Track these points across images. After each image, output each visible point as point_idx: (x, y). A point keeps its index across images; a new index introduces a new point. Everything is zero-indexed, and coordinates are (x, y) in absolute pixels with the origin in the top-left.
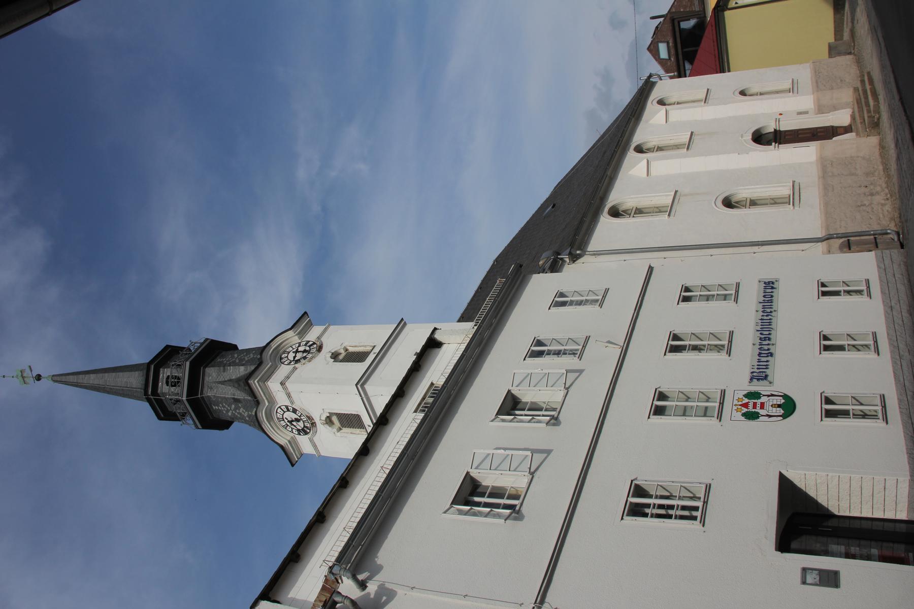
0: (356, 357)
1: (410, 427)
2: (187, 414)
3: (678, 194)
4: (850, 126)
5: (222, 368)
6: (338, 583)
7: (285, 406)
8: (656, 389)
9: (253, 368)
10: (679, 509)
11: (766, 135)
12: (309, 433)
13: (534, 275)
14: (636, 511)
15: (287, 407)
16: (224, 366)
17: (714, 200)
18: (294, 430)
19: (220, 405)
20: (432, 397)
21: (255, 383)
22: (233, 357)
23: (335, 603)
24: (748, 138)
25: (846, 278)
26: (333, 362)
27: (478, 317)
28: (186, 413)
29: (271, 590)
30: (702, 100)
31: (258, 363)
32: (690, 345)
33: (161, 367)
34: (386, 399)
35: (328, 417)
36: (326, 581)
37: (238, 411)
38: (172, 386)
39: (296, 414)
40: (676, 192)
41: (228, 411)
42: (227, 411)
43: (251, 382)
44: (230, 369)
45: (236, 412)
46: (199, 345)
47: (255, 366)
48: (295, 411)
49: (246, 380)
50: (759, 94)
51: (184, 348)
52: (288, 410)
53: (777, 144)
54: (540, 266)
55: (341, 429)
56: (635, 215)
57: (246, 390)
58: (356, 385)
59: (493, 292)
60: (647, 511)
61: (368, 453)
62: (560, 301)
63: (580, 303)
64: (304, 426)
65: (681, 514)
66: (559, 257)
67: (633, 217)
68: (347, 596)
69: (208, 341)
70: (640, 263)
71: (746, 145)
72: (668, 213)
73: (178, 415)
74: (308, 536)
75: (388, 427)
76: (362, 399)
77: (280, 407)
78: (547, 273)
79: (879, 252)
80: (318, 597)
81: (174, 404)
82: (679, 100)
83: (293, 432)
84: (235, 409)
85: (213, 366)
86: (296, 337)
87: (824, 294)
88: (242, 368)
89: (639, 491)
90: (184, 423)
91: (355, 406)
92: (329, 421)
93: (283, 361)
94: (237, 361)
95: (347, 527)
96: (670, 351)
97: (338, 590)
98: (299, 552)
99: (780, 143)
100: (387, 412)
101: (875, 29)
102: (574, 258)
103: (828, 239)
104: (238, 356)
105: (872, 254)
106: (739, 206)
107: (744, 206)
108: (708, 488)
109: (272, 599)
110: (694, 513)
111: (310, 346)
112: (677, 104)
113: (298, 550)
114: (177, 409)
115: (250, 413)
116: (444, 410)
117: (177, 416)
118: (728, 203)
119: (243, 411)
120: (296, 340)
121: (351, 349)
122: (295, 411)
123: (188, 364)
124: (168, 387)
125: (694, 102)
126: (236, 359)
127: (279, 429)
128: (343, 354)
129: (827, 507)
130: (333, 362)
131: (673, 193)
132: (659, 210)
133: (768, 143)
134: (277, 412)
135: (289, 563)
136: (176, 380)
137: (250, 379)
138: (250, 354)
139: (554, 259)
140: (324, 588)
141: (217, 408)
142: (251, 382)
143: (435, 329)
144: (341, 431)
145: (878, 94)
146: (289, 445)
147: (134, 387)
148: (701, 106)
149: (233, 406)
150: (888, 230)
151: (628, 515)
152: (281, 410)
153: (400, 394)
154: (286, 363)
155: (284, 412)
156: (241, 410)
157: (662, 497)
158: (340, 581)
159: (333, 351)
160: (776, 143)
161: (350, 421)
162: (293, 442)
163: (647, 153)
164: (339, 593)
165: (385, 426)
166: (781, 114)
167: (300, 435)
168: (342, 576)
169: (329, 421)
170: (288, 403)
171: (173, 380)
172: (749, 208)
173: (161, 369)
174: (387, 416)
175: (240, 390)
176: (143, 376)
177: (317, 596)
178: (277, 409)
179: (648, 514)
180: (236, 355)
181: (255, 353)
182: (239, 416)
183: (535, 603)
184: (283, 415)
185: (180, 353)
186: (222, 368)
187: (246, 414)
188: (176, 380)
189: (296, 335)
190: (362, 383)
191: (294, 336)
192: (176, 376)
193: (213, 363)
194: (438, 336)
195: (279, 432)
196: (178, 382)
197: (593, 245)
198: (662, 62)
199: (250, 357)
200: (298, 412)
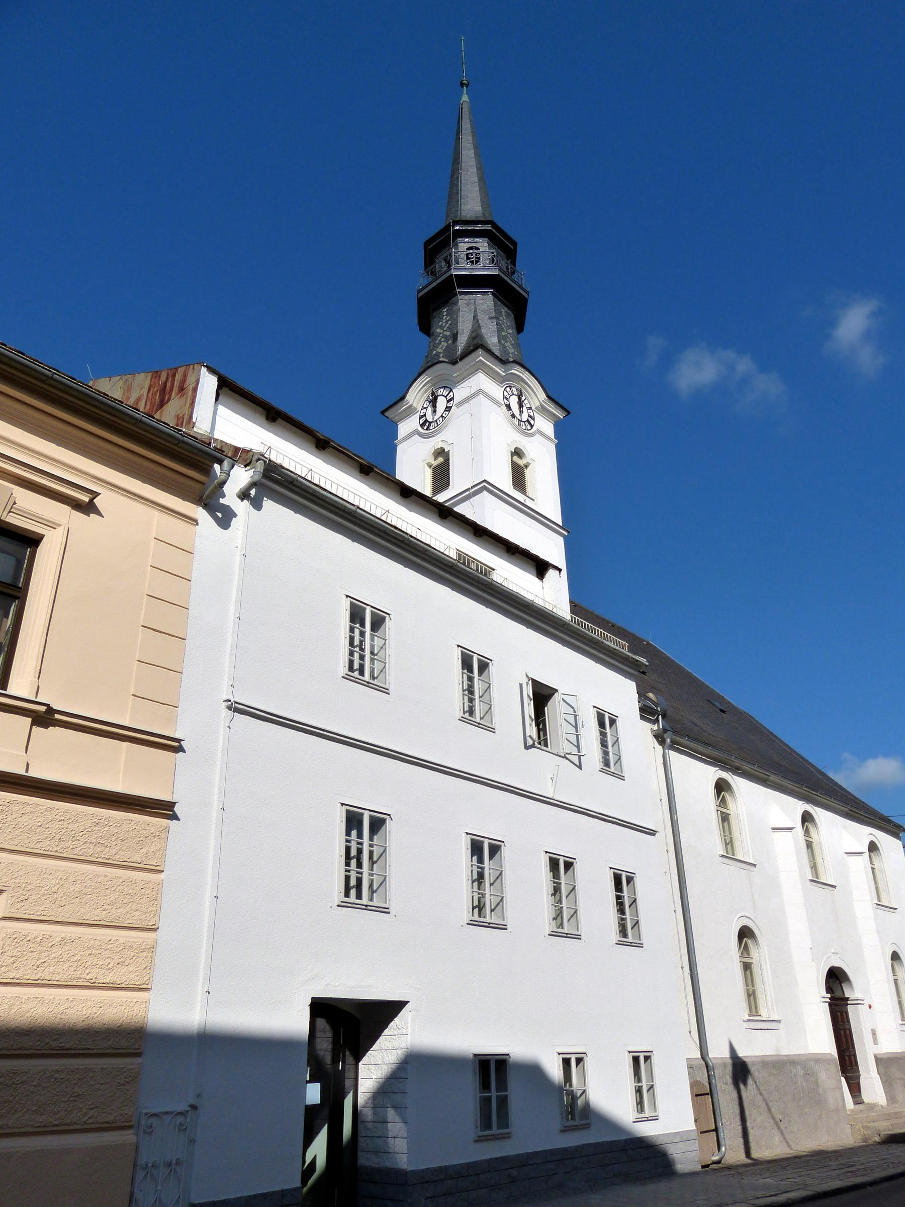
0: (519, 477)
2: (434, 277)
3: (752, 868)
4: (862, 1102)
5: (493, 314)
6: (246, 466)
8: (503, 842)
9: (497, 353)
10: (357, 875)
11: (840, 988)
12: (423, 429)
13: (635, 683)
14: (353, 820)
15: (452, 399)
16: (496, 318)
17: (746, 915)
18: (425, 410)
19: (448, 318)
21: (480, 356)
22: (508, 327)
23: (220, 462)
25: (658, 1089)
28: (435, 275)
29: (231, 390)
30: (879, 900)
31: (503, 358)
32: (560, 884)
33: (489, 239)
34: (469, 515)
35: (444, 450)
36: (247, 452)
37: (443, 340)
38: (467, 255)
39: (445, 411)
40: (755, 865)
41: (442, 327)
42: (441, 326)
43: (480, 351)
44: (493, 326)
45: (442, 337)
47: (499, 356)
48: (448, 409)
49: (481, 345)
50: (896, 978)
51: (515, 265)
52: (448, 401)
53: (828, 1000)
54: (646, 695)
55: (430, 467)
56: (719, 812)
57: (470, 347)
58: (485, 481)
59: (610, 637)
60: (354, 833)
61: (405, 498)
62: (606, 721)
63: (604, 744)
65: (352, 877)
66: (660, 717)
67: (717, 810)
68: (229, 476)
69: (526, 295)
70: (658, 819)
71: (824, 960)
72: (725, 855)
73: (432, 267)
74: (236, 395)
76: (468, 489)
78: (639, 702)
79: (695, 1135)
80: (226, 443)
81: (445, 260)
82: (876, 871)
83: (422, 409)
84: (445, 337)
85: (495, 304)
86: (538, 404)
87: (636, 1060)
88: (495, 340)
89: (377, 824)
91: (459, 482)
92: (441, 453)
93: (508, 389)
94: (504, 334)
95: (313, 472)
96: (551, 859)
97: (236, 466)
98: (279, 420)
99: (830, 1005)
100: (488, 536)
102: (659, 737)
103: (707, 1065)
105: (692, 1126)
106: (742, 948)
107: (742, 954)
108: (385, 911)
109: (220, 391)
110: (353, 892)
111: (528, 421)
112: (872, 868)
113: (281, 420)
114: (440, 265)
115: (441, 355)
117: (430, 266)
118: (745, 934)
119: (443, 346)
120: (535, 403)
121: (527, 472)
122: (448, 409)
123: (496, 272)
124: (465, 250)
125: (877, 889)
126: (506, 332)
127: (425, 392)
128: (521, 462)
129: (382, 1035)
131: (751, 861)
132: (729, 843)
133: (829, 989)
135: (263, 408)
137: (483, 351)
138: (514, 348)
139: (657, 710)
140: (237, 449)
142: (480, 351)
143: (560, 570)
144: (427, 467)
146: (406, 406)
147: (462, 207)
148: (872, 900)
149: (448, 333)
150: (725, 1148)
151: (348, 812)
153: (479, 533)
154: (506, 393)
155: (446, 397)
156: (445, 344)
157: (371, 853)
158: (248, 468)
160: (830, 999)
161: (441, 476)
162: (411, 411)
163: (803, 827)
164: (233, 466)
166: (870, 1007)
167: (420, 418)
168: (253, 470)
169: (441, 453)
170: (456, 400)
172: (740, 962)
173: (487, 239)
175: (468, 340)
176: (476, 217)
177: (227, 442)
179: (350, 836)
180: (510, 331)
181: (516, 355)
182: (437, 342)
183: (236, 702)
184: (442, 395)
185: (508, 260)
186: (493, 314)
187: (439, 350)
189: (540, 403)
190: (485, 487)
191: (539, 401)
192: (479, 258)
193: (499, 303)
194: (551, 573)
195: (421, 392)
197: (675, 757)
200: (447, 413)
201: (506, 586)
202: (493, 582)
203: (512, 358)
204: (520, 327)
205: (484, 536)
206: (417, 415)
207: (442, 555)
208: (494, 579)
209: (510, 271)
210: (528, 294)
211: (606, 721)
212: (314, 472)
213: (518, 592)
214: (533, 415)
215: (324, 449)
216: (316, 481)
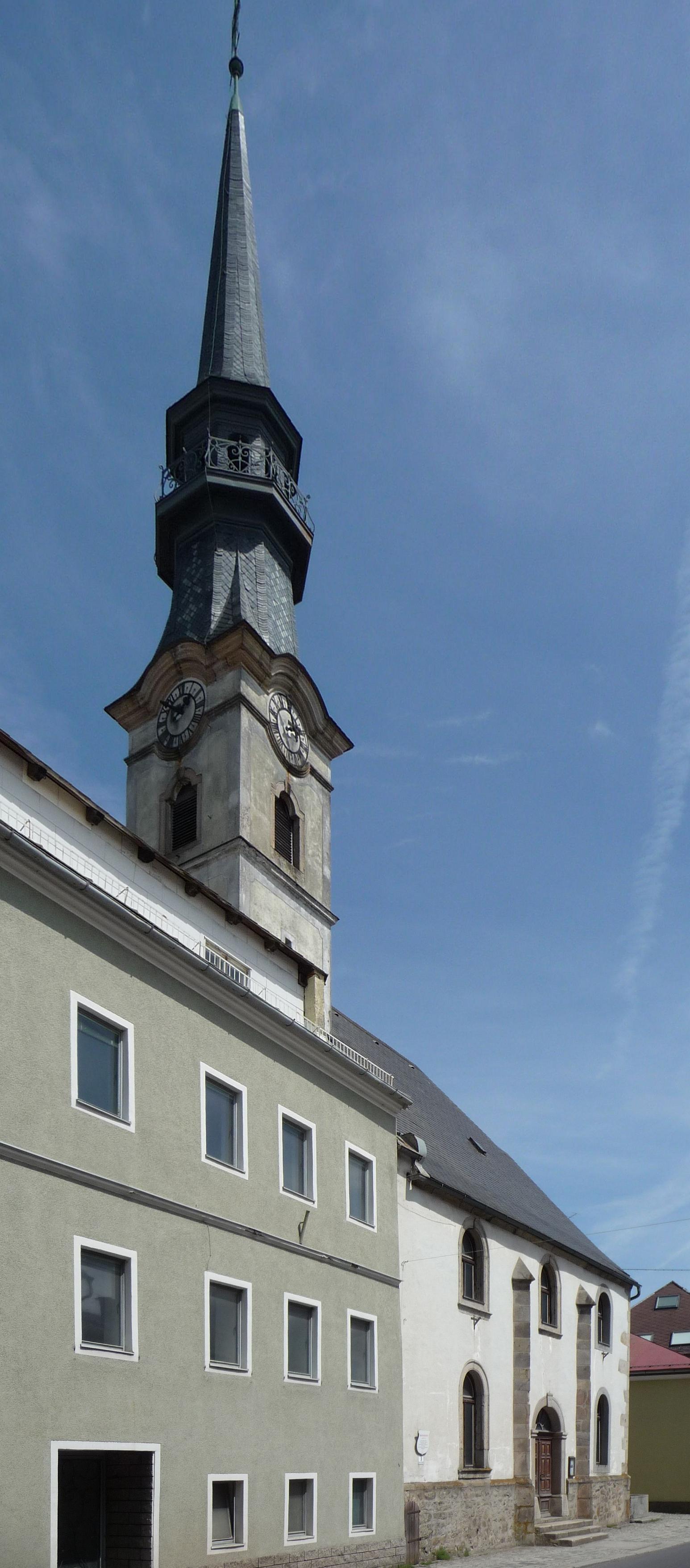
1: (154, 912)
7: (204, 700)
20: (207, 953)
24: (551, 1341)
26: (276, 797)
27: (342, 1045)
46: (302, 516)
64: (173, 736)
69: (309, 540)
75: (135, 859)
77: (202, 689)
90: (163, 473)
98: (277, 951)
101: (657, 1544)
104: (283, 604)
116: (146, 959)
130: (276, 797)
134: (194, 682)
135: (297, 962)
136: (240, 459)
141: (195, 553)
143: (325, 976)
145: (582, 1545)
152: (197, 691)
159: (292, 796)
165: (136, 857)
171: (240, 451)
174: (199, 895)
178: (200, 685)
188: (240, 459)
196: (236, 464)
198: (653, 1299)
199: (283, 630)
201: (264, 999)
202: (250, 993)
203: (285, 646)
204: (297, 597)
205: (239, 924)
206: (155, 721)
207: (198, 959)
208: (251, 990)
209: (289, 491)
210: (312, 539)
211: (360, 1163)
212: (33, 825)
213: (277, 1007)
214: (271, 714)
215: (97, 824)
216: (36, 840)
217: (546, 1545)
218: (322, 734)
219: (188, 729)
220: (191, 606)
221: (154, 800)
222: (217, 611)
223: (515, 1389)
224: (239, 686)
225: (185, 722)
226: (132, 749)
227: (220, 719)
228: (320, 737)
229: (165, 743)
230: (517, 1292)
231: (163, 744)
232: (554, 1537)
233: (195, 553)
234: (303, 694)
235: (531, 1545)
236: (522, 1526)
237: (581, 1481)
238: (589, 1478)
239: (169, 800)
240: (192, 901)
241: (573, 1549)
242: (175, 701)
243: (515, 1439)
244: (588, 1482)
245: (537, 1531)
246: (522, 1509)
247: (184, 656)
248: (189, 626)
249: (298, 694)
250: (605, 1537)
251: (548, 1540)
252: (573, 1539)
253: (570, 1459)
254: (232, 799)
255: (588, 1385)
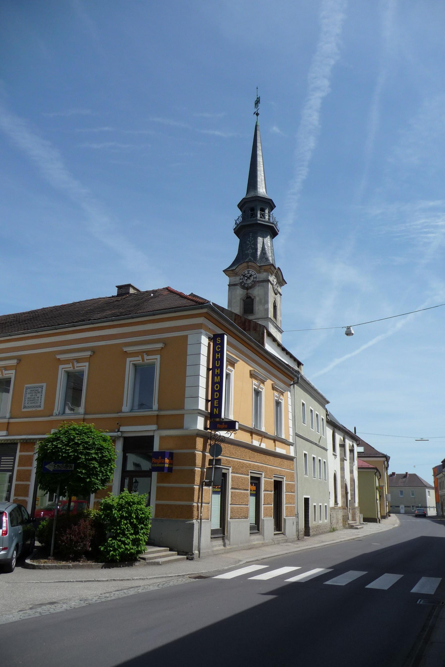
64: (245, 284)
77: (255, 274)
141: (251, 236)
217: (351, 529)
218: (281, 282)
219: (251, 283)
220: (250, 249)
221: (238, 298)
222: (259, 253)
223: (341, 478)
224: (268, 277)
225: (249, 281)
226: (230, 282)
227: (261, 284)
228: (280, 283)
229: (243, 285)
230: (340, 448)
231: (242, 284)
232: (353, 526)
233: (251, 236)
234: (278, 274)
235: (347, 528)
236: (345, 522)
237: (352, 508)
238: (354, 507)
239: (244, 300)
240: (287, 356)
241: (359, 530)
242: (246, 274)
243: (341, 494)
244: (354, 509)
245: (349, 524)
246: (344, 517)
247: (250, 265)
248: (250, 255)
249: (278, 274)
250: (362, 528)
251: (352, 527)
252: (358, 527)
253: (350, 500)
254: (266, 306)
255: (353, 476)
